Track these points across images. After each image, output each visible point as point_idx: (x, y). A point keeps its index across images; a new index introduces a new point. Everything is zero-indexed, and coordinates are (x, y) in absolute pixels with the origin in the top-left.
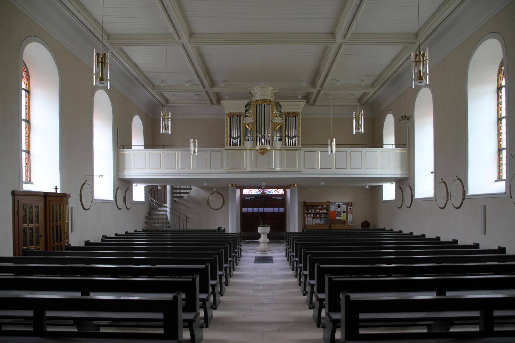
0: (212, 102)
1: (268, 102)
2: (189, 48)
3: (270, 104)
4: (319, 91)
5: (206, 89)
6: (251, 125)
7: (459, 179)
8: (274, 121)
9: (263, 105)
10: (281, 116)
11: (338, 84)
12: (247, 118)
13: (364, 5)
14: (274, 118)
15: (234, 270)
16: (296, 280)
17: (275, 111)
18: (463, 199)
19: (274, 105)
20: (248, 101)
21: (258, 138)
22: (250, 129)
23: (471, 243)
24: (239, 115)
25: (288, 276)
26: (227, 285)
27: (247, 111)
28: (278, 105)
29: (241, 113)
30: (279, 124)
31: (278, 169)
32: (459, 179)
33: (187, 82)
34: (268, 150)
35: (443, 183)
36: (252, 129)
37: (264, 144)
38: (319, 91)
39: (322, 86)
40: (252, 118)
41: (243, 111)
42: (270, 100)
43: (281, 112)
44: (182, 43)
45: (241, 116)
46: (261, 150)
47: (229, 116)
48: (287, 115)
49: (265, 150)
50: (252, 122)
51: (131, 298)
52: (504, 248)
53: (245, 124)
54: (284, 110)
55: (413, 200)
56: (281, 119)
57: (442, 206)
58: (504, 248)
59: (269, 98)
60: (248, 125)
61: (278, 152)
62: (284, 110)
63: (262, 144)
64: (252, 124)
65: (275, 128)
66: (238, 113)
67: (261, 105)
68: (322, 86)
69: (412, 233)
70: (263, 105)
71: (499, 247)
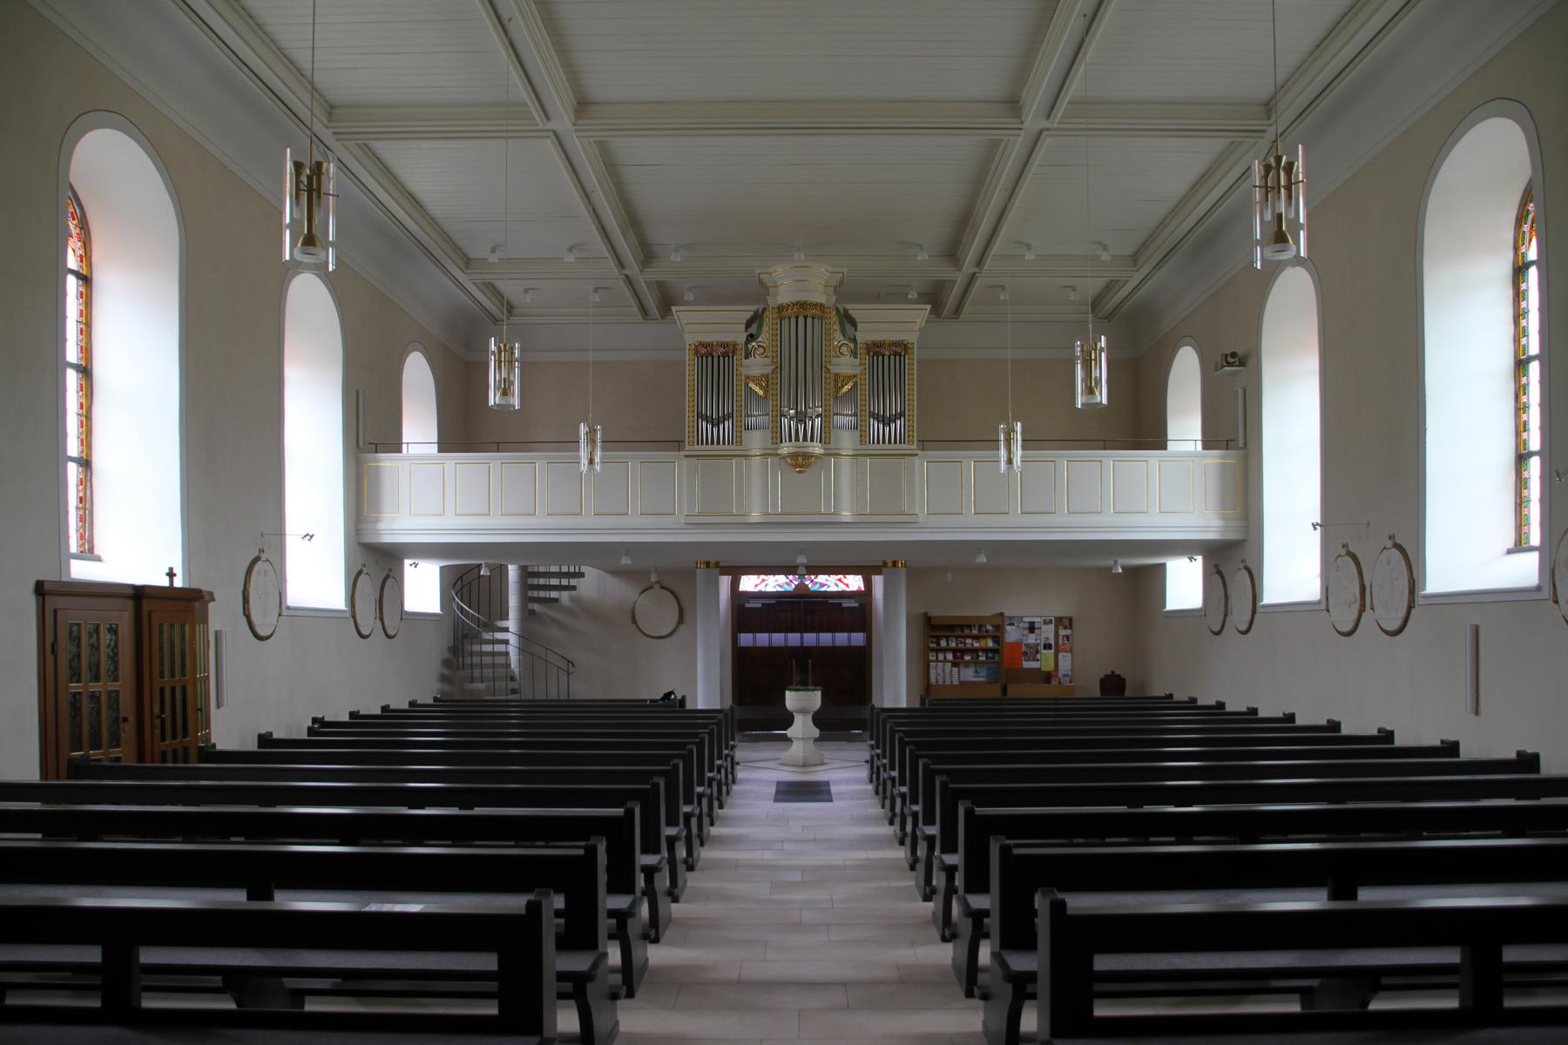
0: (644, 312)
1: (816, 312)
2: (576, 145)
3: (821, 318)
4: (972, 277)
5: (626, 272)
6: (765, 381)
7: (1398, 547)
8: (834, 370)
9: (801, 320)
10: (854, 354)
11: (1030, 256)
12: (751, 360)
13: (1108, 15)
14: (834, 360)
15: (712, 824)
16: (901, 854)
17: (838, 339)
18: (1410, 608)
19: (834, 319)
20: (755, 308)
21: (785, 421)
22: (761, 393)
23: (1433, 740)
24: (728, 350)
25: (877, 842)
26: (691, 868)
27: (751, 337)
28: (848, 320)
29: (735, 345)
30: (850, 378)
31: (846, 515)
32: (1398, 547)
33: (570, 250)
34: (817, 457)
35: (1348, 559)
36: (766, 392)
37: (805, 439)
38: (972, 277)
39: (980, 262)
40: (768, 361)
41: (741, 338)
42: (821, 305)
43: (854, 340)
44: (555, 132)
45: (734, 353)
46: (794, 456)
47: (697, 353)
48: (875, 349)
49: (807, 456)
50: (768, 370)
51: (399, 908)
52: (1536, 757)
53: (747, 377)
54: (863, 336)
55: (1259, 610)
56: (857, 361)
57: (1347, 628)
58: (1536, 757)
59: (819, 298)
60: (756, 380)
61: (846, 463)
62: (863, 336)
63: (797, 439)
64: (767, 377)
65: (838, 389)
66: (724, 345)
67: (793, 320)
68: (980, 262)
69: (1254, 711)
70: (801, 320)
71: (1519, 753)
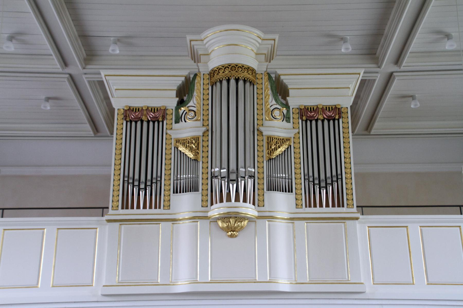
0: (96, 128)
1: (249, 76)
2: (85, 82)
3: (252, 83)
4: (390, 77)
5: (70, 70)
6: (193, 143)
8: (267, 132)
9: (233, 82)
10: (287, 118)
11: (449, 45)
12: (182, 124)
13: (417, 35)
14: (267, 123)
17: (271, 102)
19: (266, 84)
20: (186, 73)
21: (216, 181)
22: (191, 155)
24: (158, 117)
27: (181, 103)
28: (281, 90)
29: (165, 110)
30: (283, 141)
31: (284, 285)
33: (48, 99)
34: (250, 220)
36: (197, 154)
37: (237, 199)
38: (390, 77)
39: (398, 61)
40: (199, 123)
41: (171, 102)
42: (253, 70)
43: (287, 106)
44: (71, 75)
45: (164, 118)
46: (225, 218)
47: (125, 117)
48: (308, 115)
49: (239, 218)
50: (199, 132)
53: (178, 141)
54: (296, 100)
56: (290, 125)
59: (252, 63)
60: (184, 142)
61: (281, 229)
62: (296, 100)
63: (229, 200)
64: (197, 139)
65: (271, 152)
66: (154, 110)
67: (225, 83)
68: (398, 61)
70: (233, 82)
